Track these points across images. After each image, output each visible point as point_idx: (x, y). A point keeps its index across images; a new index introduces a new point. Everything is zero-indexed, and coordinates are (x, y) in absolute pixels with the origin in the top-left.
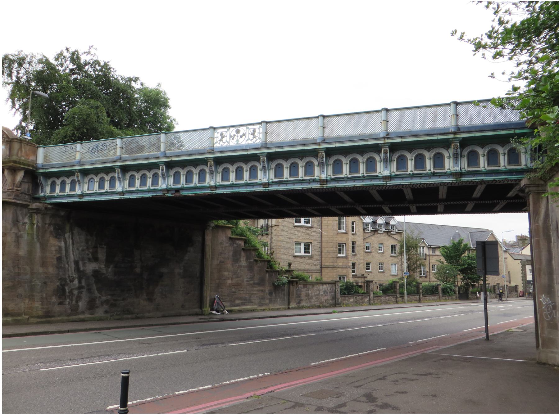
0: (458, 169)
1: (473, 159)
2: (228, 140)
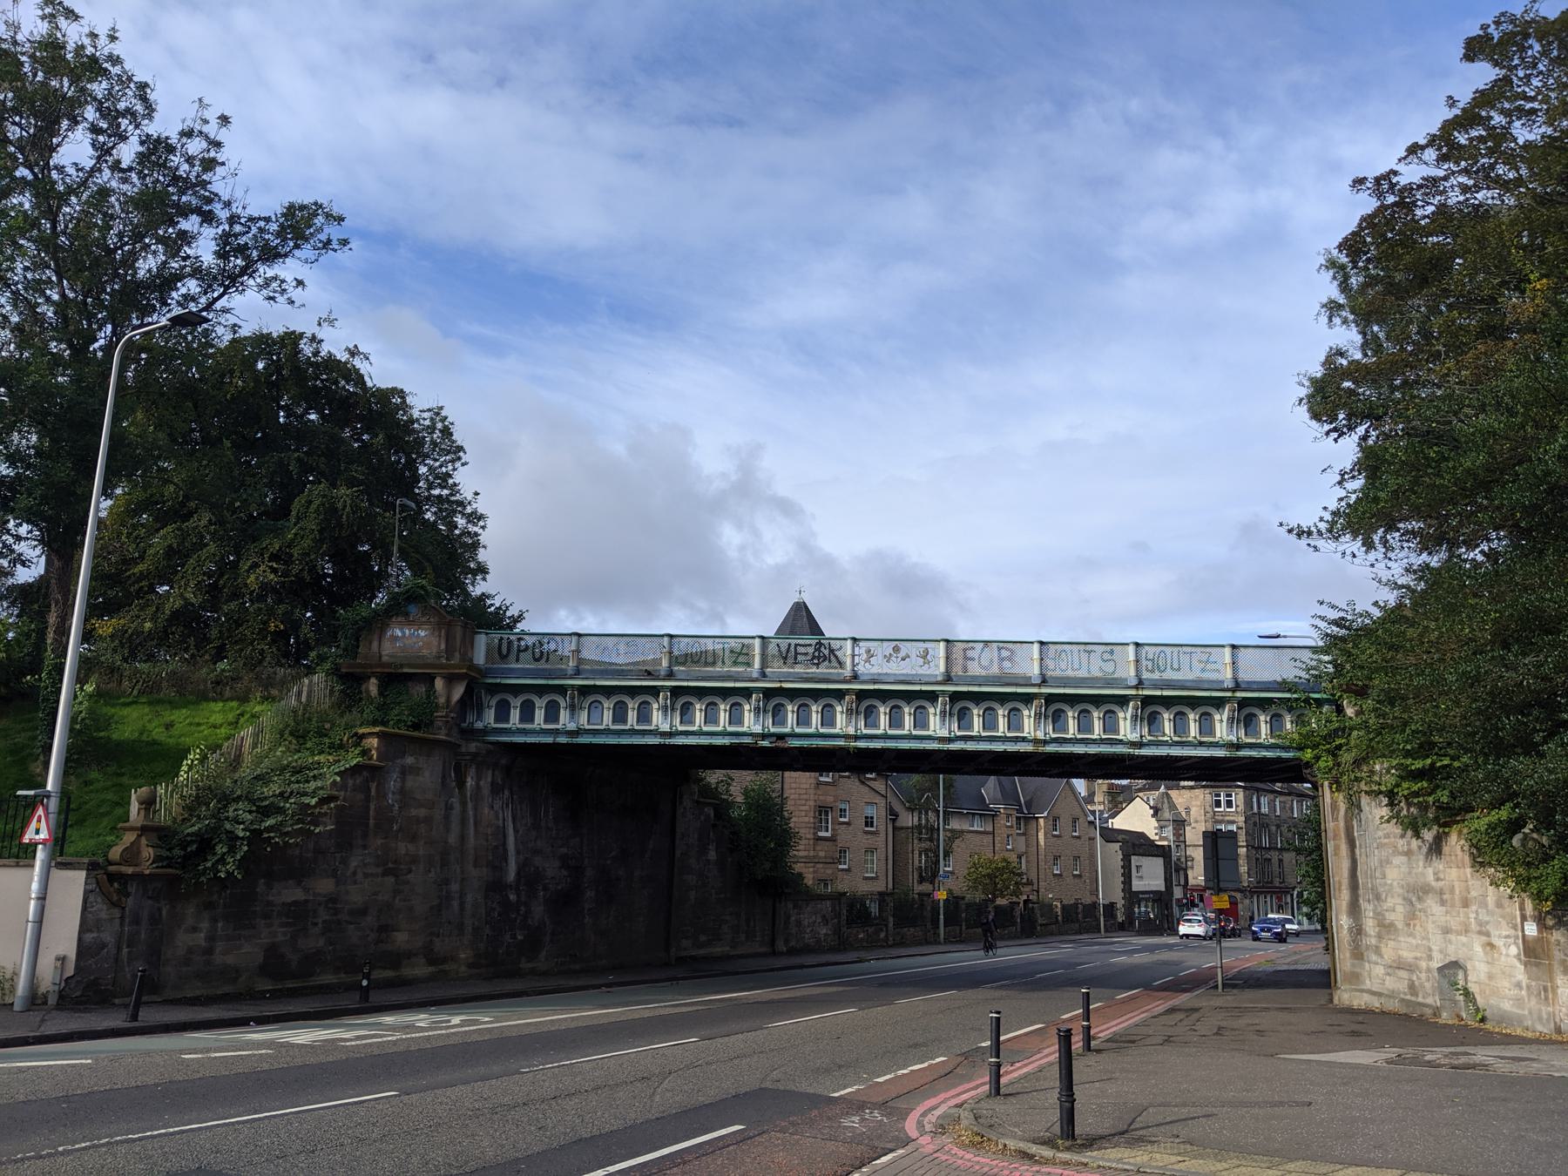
1: (778, 713)
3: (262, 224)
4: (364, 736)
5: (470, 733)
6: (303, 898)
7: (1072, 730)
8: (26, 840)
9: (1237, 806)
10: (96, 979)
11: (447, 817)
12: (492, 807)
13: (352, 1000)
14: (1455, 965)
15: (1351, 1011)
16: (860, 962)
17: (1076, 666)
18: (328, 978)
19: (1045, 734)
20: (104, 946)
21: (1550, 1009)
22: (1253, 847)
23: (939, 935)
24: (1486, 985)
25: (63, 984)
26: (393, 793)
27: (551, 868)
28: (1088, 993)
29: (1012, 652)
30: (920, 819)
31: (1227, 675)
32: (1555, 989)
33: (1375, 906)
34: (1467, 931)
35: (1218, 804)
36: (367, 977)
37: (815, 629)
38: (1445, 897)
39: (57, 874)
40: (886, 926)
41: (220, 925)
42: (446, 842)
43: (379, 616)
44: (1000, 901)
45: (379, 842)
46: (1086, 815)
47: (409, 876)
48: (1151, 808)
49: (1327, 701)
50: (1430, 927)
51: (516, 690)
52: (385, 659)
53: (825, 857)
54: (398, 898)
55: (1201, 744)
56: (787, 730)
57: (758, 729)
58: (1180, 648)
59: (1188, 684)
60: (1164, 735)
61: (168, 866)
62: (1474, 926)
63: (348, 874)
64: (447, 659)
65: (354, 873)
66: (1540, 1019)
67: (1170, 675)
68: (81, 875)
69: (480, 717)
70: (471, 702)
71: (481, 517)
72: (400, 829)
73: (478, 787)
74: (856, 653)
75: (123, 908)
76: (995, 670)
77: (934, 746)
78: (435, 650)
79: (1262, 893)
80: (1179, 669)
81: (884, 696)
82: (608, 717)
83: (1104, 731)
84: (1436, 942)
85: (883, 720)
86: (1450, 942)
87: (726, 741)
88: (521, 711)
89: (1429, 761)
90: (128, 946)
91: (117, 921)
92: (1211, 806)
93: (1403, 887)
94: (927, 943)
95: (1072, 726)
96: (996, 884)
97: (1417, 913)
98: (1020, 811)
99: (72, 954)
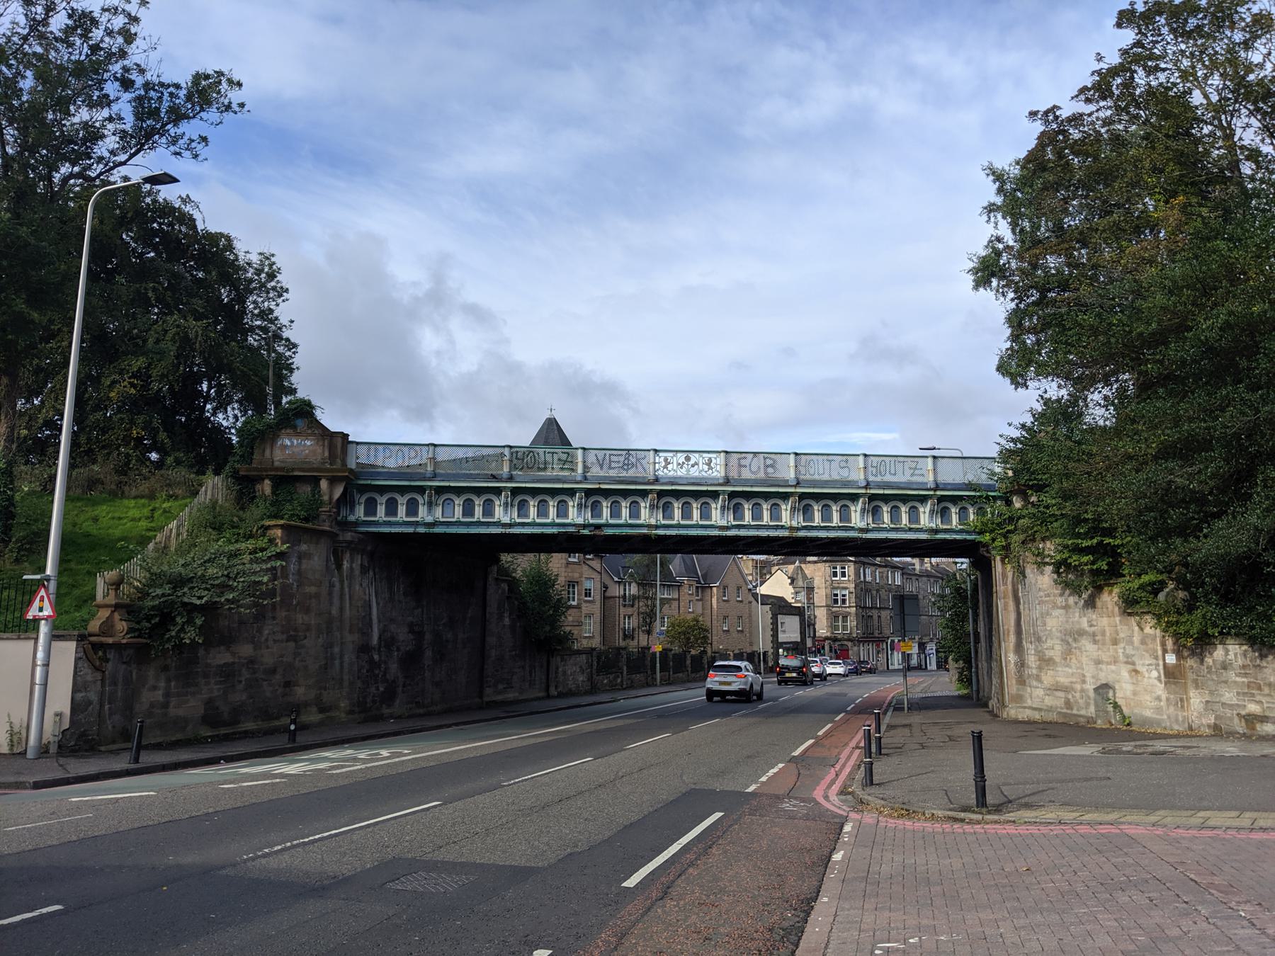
0: (934, 526)
1: (596, 509)
2: (675, 468)
3: (171, 89)
4: (269, 528)
5: (345, 525)
6: (232, 660)
7: (817, 520)
8: (30, 616)
9: (849, 576)
10: (85, 731)
11: (330, 594)
12: (361, 585)
13: (281, 741)
14: (1106, 686)
15: (1017, 722)
16: (614, 701)
17: (821, 472)
18: (250, 726)
19: (728, 522)
20: (90, 703)
21: (1186, 714)
22: (860, 607)
23: (656, 679)
24: (1132, 699)
25: (61, 736)
26: (293, 574)
27: (402, 634)
28: (879, 713)
29: (775, 461)
30: (625, 590)
31: (791, 475)
32: (1188, 699)
33: (1037, 647)
34: (1115, 662)
35: (835, 574)
36: (293, 722)
37: (565, 442)
38: (1097, 638)
39: (57, 645)
40: (622, 673)
41: (173, 684)
42: (330, 613)
43: (272, 428)
44: (693, 652)
45: (284, 614)
46: (747, 584)
47: (305, 641)
48: (789, 578)
49: (1000, 498)
50: (1084, 660)
51: (382, 490)
52: (276, 464)
53: (573, 621)
54: (297, 659)
55: (910, 529)
56: (603, 521)
57: (580, 521)
58: (896, 458)
59: (902, 485)
60: (884, 523)
61: (139, 637)
62: (1121, 658)
63: (263, 639)
64: (331, 464)
65: (267, 640)
66: (1177, 721)
67: (888, 478)
68: (72, 645)
69: (352, 510)
70: (347, 501)
71: (295, 346)
72: (298, 603)
73: (351, 569)
74: (657, 461)
75: (104, 672)
76: (761, 475)
77: (716, 533)
78: (319, 458)
79: (866, 641)
80: (895, 474)
81: (677, 494)
82: (458, 512)
83: (841, 521)
84: (1089, 671)
85: (677, 513)
86: (1101, 670)
87: (555, 530)
88: (386, 507)
89: (1095, 541)
90: (109, 703)
91: (99, 683)
92: (830, 576)
93: (1061, 631)
94: (648, 685)
95: (817, 516)
96: (689, 639)
97: (1073, 650)
98: (698, 582)
99: (67, 710)
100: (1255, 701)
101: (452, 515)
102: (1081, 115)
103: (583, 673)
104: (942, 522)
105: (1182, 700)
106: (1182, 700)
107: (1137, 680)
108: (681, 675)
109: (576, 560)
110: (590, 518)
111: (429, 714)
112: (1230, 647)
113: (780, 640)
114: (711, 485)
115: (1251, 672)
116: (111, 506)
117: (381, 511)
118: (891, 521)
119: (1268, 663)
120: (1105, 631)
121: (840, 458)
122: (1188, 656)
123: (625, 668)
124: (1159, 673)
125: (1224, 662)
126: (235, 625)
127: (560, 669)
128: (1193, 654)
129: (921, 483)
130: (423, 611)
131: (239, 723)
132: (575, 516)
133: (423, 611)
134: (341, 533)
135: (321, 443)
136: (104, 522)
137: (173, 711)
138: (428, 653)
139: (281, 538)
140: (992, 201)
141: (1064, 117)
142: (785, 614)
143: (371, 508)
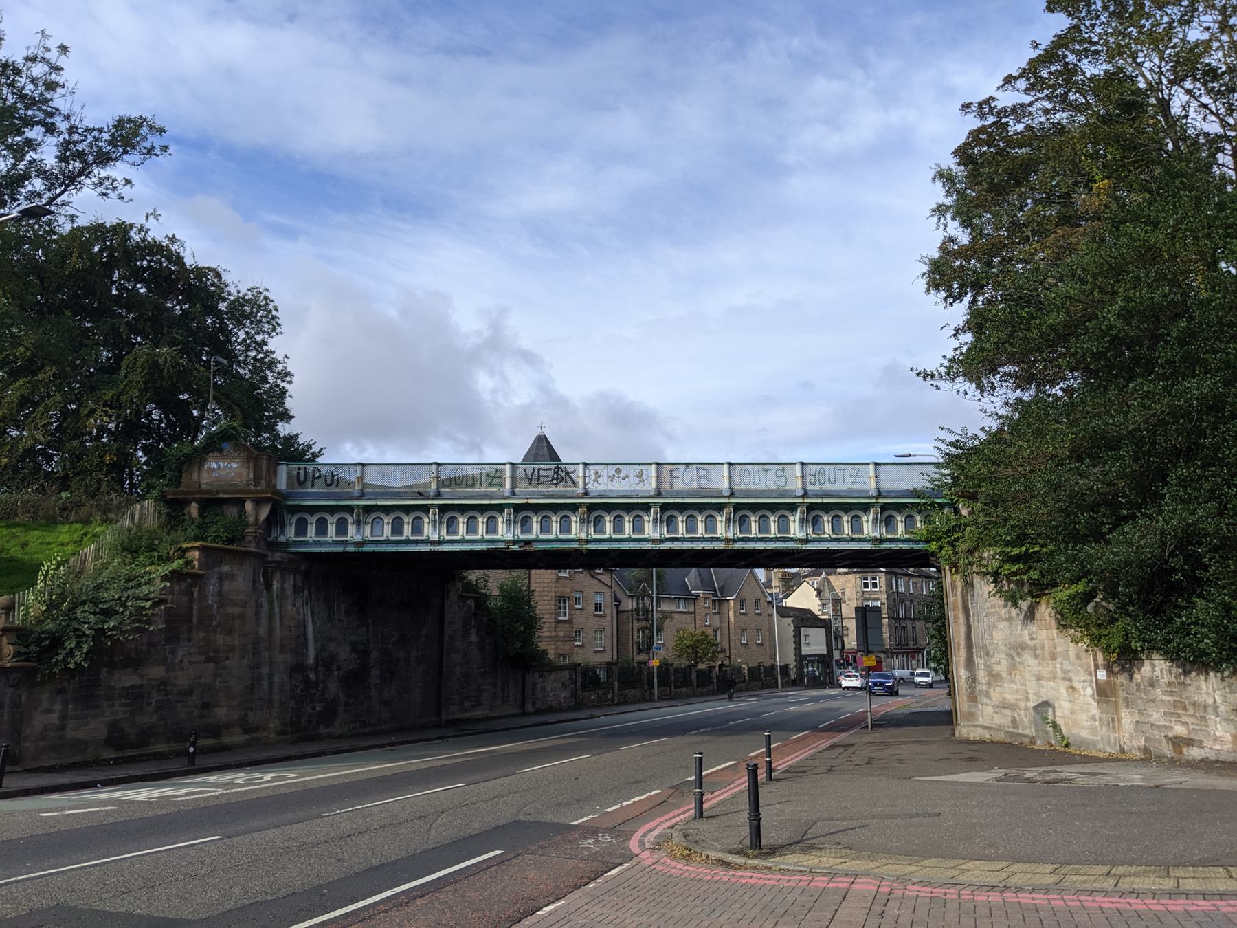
3: (96, 133)
4: (187, 550)
5: (275, 546)
6: (139, 682)
7: (754, 530)
9: (880, 587)
11: (257, 614)
12: (294, 605)
13: (182, 764)
14: (1046, 704)
15: (968, 742)
18: (161, 747)
19: (734, 535)
22: (893, 618)
23: (653, 694)
24: (1069, 718)
26: (212, 595)
27: (344, 653)
29: (708, 471)
30: (638, 604)
31: (725, 486)
32: (1119, 719)
35: (866, 585)
36: (193, 744)
37: (554, 456)
38: (1037, 652)
40: (613, 689)
44: (701, 666)
45: (201, 635)
46: (766, 597)
47: (227, 662)
48: (815, 590)
50: (1027, 675)
51: (312, 510)
52: (203, 487)
53: (564, 636)
55: (853, 539)
56: (533, 537)
57: (509, 537)
58: (835, 466)
59: (842, 494)
60: (824, 533)
61: (26, 660)
63: (177, 661)
64: (255, 486)
66: (1109, 742)
67: (828, 487)
69: (283, 532)
70: (275, 520)
72: (219, 625)
73: (283, 589)
74: (587, 475)
76: (694, 486)
78: (245, 479)
79: (900, 653)
81: (609, 508)
82: (387, 530)
83: (779, 531)
84: (1032, 687)
85: (609, 527)
86: (1043, 687)
87: (484, 547)
88: (296, 526)
93: (1006, 645)
94: (644, 700)
95: (682, 527)
100: (1181, 722)
101: (381, 534)
102: (1022, 105)
103: (566, 689)
104: (887, 531)
105: (1113, 720)
106: (1113, 720)
107: (1074, 698)
108: (684, 690)
109: (566, 575)
110: (519, 534)
111: (376, 734)
112: (1156, 662)
113: (803, 653)
114: (642, 497)
115: (1176, 690)
116: (44, 531)
117: (311, 530)
118: (833, 531)
119: (1192, 680)
120: (1044, 644)
121: (776, 467)
122: (1118, 672)
123: (616, 683)
124: (1093, 690)
125: (1151, 678)
126: (144, 648)
127: (539, 686)
128: (1123, 670)
129: (861, 491)
130: (368, 631)
131: (148, 746)
132: (504, 532)
133: (368, 631)
134: (270, 554)
135: (246, 465)
136: (33, 547)
137: (69, 734)
138: (375, 672)
139: (199, 560)
140: (941, 203)
141: (999, 107)
142: (809, 627)
143: (301, 528)
